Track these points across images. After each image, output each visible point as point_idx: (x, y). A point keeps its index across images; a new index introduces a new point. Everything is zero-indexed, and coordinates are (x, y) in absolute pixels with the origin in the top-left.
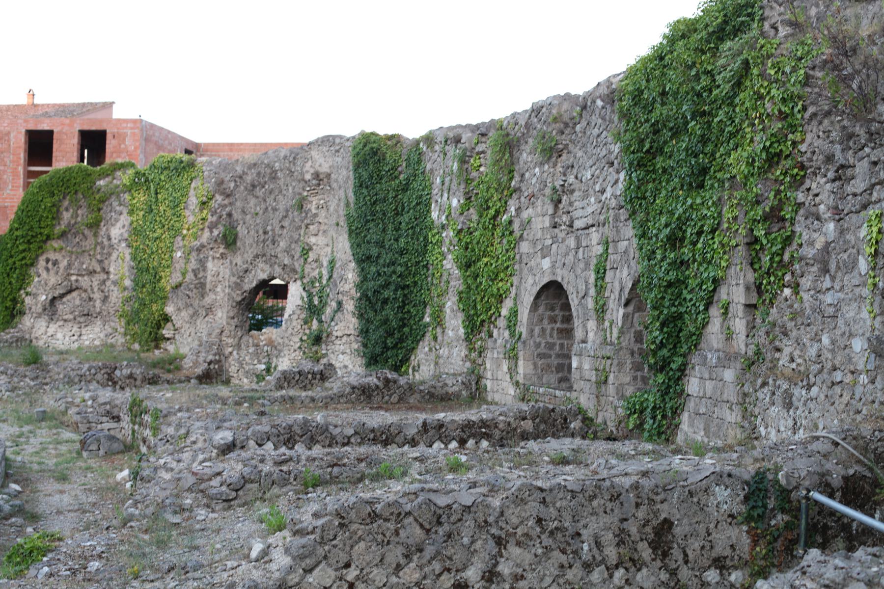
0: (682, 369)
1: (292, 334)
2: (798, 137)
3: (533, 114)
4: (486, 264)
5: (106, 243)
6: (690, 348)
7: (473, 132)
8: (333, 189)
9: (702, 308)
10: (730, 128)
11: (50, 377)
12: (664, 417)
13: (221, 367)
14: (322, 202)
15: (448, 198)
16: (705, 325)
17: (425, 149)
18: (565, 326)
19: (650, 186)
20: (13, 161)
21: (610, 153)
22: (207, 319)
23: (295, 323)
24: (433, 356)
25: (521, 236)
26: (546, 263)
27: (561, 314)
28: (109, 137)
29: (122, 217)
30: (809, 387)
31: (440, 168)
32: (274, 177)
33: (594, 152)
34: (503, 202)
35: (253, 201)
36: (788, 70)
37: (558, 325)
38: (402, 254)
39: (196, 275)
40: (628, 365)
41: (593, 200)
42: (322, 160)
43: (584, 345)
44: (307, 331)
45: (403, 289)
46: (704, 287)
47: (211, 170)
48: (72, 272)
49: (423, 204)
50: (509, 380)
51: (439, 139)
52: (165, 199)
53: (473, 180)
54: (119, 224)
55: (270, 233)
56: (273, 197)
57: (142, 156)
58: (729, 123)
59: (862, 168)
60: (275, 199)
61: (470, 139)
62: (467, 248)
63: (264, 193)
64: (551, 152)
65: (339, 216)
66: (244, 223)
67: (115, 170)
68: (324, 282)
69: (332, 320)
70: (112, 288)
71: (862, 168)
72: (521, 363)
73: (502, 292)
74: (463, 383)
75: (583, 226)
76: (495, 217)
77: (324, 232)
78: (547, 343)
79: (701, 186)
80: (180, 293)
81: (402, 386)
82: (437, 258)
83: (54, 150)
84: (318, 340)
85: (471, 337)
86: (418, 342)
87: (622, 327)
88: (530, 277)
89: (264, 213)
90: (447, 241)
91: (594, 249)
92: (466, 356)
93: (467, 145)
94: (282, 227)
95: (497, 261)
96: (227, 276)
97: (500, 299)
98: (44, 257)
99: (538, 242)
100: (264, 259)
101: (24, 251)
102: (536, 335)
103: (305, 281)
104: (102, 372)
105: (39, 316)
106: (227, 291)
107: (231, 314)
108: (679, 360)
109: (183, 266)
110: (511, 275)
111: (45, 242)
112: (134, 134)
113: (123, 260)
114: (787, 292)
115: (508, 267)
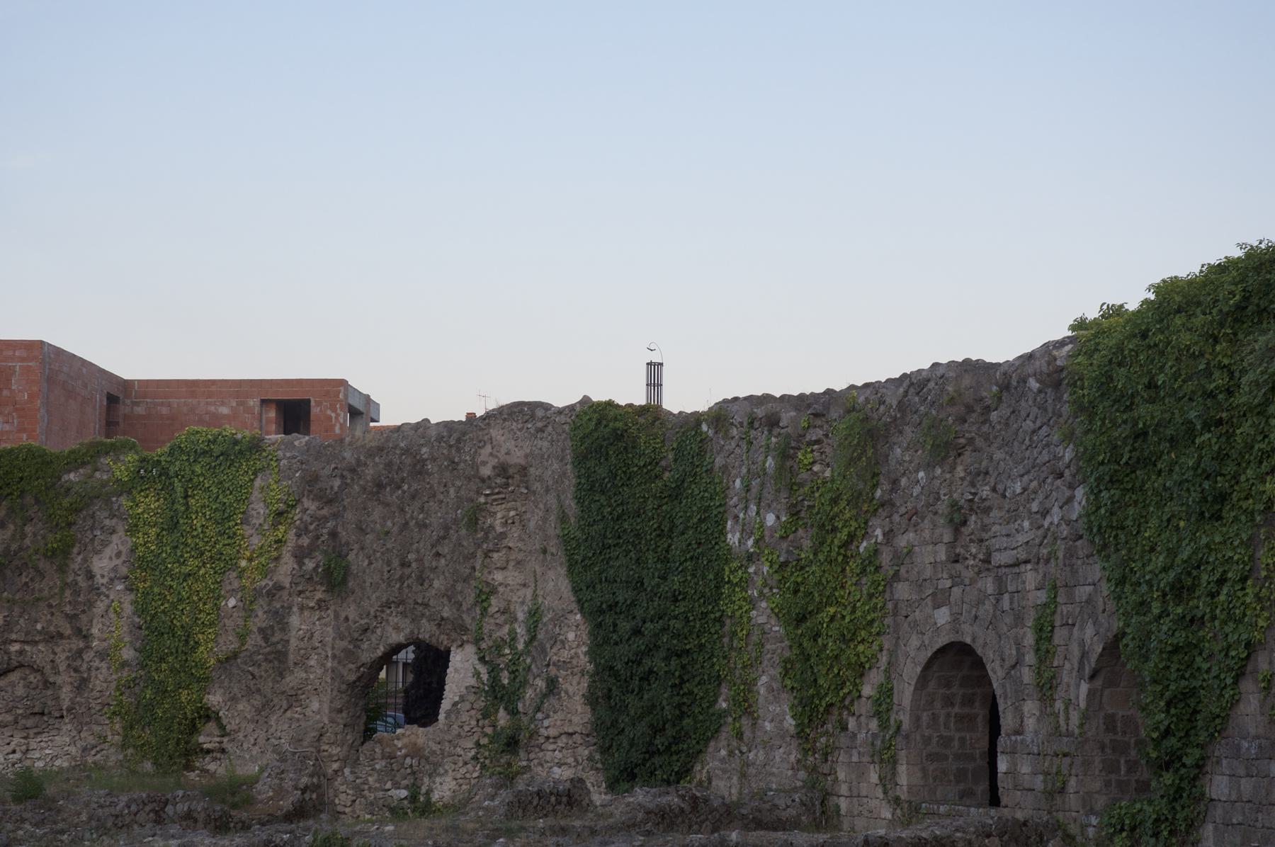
0: (1199, 766)
1: (459, 735)
3: (912, 390)
4: (832, 619)
5: (82, 582)
6: (1212, 735)
7: (797, 409)
8: (534, 493)
9: (1229, 681)
10: (1262, 446)
11: (64, 820)
12: (1172, 833)
13: (321, 796)
14: (512, 513)
15: (758, 513)
16: (1235, 702)
17: (711, 433)
18: (966, 710)
19: (1131, 511)
21: (1058, 458)
22: (289, 714)
23: (465, 717)
24: (736, 764)
25: (896, 573)
26: (942, 616)
27: (961, 692)
29: (115, 538)
31: (737, 469)
32: (419, 470)
33: (1027, 454)
34: (861, 520)
35: (377, 512)
37: (956, 709)
38: (676, 600)
39: (266, 639)
41: (1026, 524)
42: (510, 445)
43: (1019, 738)
44: (489, 730)
45: (679, 656)
46: (1233, 653)
47: (294, 457)
48: (14, 637)
49: (713, 521)
50: (881, 796)
51: (738, 419)
52: (203, 506)
53: (801, 485)
54: (108, 552)
55: (414, 565)
56: (417, 504)
57: (43, 411)
58: (1260, 438)
60: (422, 509)
62: (796, 592)
64: (944, 450)
66: (362, 548)
68: (521, 646)
69: (538, 709)
70: (97, 663)
72: (902, 768)
73: (863, 660)
74: (803, 804)
75: (1010, 562)
76: (845, 545)
77: (519, 563)
78: (941, 737)
80: (235, 671)
81: (716, 809)
82: (740, 608)
85: (808, 730)
86: (708, 740)
87: (1087, 709)
88: (914, 637)
89: (401, 531)
90: (759, 581)
91: (1030, 596)
92: (798, 761)
93: (789, 430)
94: (438, 555)
95: (853, 612)
96: (329, 639)
97: (861, 670)
99: (927, 584)
100: (401, 609)
102: (924, 724)
103: (484, 646)
104: (147, 808)
106: (329, 664)
108: (1197, 753)
109: (241, 622)
110: (878, 634)
113: (118, 614)
115: (873, 621)
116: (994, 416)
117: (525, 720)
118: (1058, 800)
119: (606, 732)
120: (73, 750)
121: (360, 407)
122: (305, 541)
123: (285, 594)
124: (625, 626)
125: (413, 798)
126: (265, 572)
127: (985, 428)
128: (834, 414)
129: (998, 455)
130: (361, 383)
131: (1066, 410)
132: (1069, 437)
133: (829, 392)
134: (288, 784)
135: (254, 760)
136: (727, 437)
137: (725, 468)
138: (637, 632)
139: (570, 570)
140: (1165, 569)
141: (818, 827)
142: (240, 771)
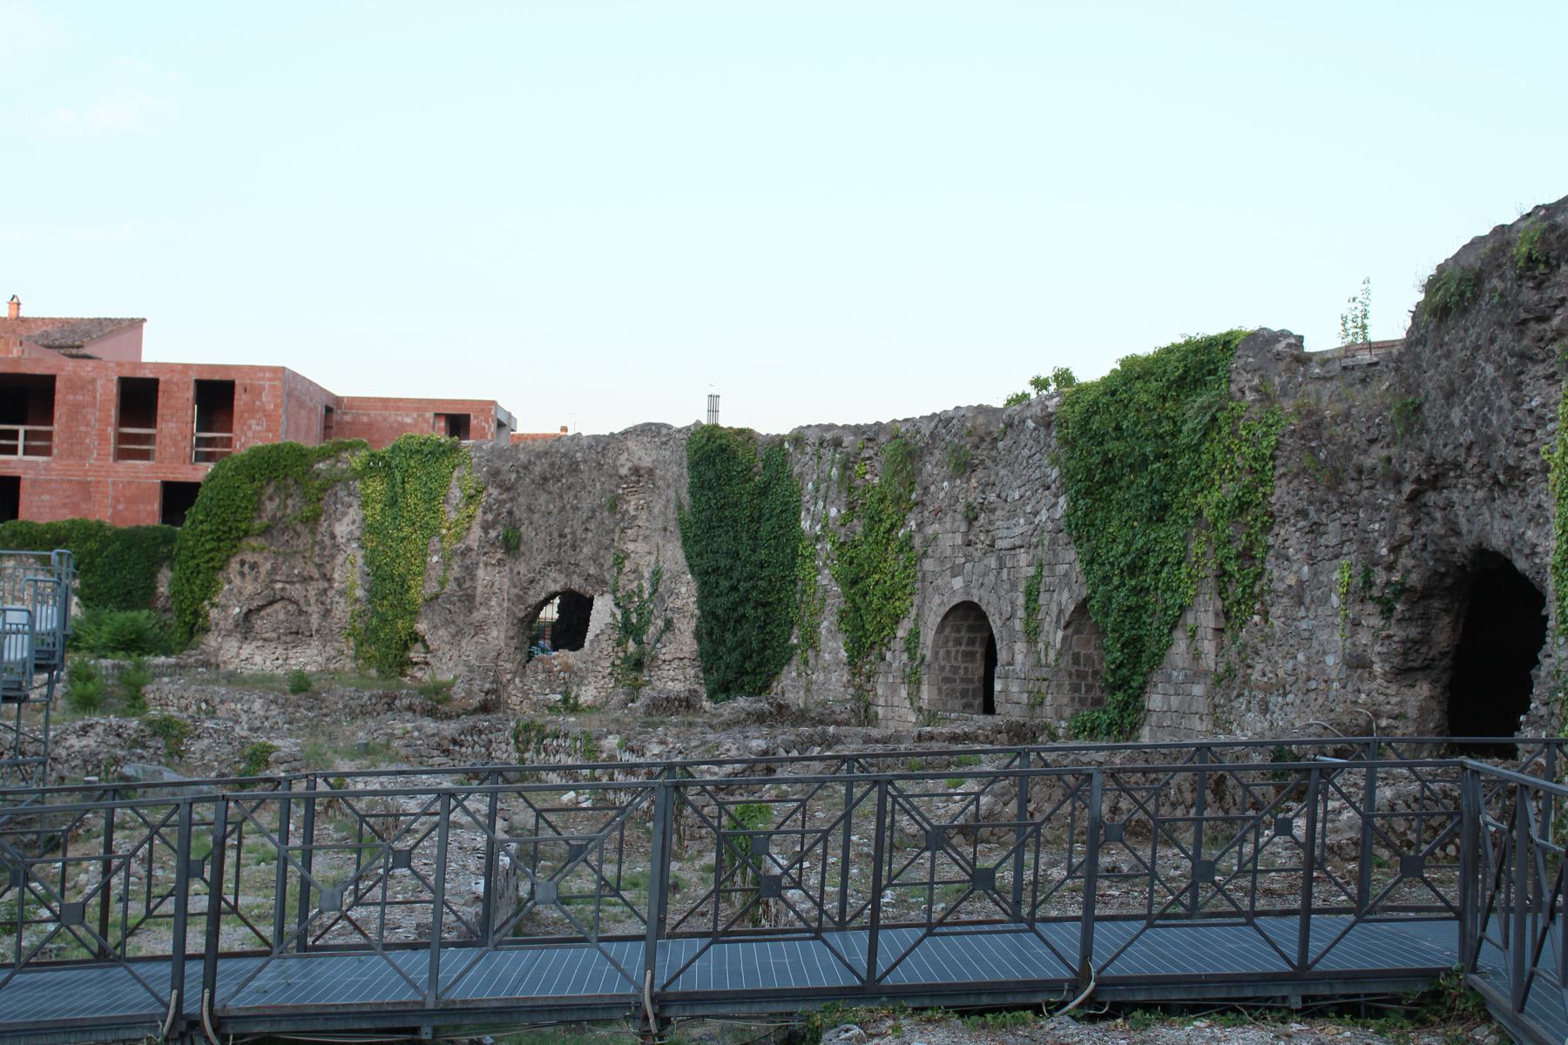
0: (1142, 688)
2: (1268, 490)
4: (877, 583)
5: (328, 542)
13: (498, 697)
16: (1169, 645)
19: (1099, 514)
20: (100, 420)
23: (604, 645)
24: (803, 682)
26: (958, 583)
28: (238, 390)
30: (1285, 695)
31: (809, 474)
32: (574, 468)
35: (543, 498)
36: (1259, 433)
37: (963, 648)
39: (459, 585)
40: (1067, 687)
41: (1022, 521)
42: (642, 453)
44: (621, 655)
49: (791, 512)
51: (811, 440)
53: (856, 488)
54: (347, 520)
56: (572, 493)
59: (1333, 527)
61: (852, 443)
62: (851, 563)
63: (560, 489)
65: (667, 520)
67: (340, 450)
68: (646, 596)
69: (658, 641)
70: (337, 599)
71: (1333, 527)
72: (925, 688)
76: (889, 531)
79: (1161, 520)
83: (160, 405)
84: (638, 665)
97: (896, 619)
98: (238, 558)
101: (211, 550)
105: (229, 634)
107: (511, 634)
108: (1141, 679)
111: (239, 539)
112: (274, 387)
114: (1256, 618)
116: (1000, 445)
117: (648, 648)
118: (1038, 710)
119: (708, 658)
120: (319, 659)
121: (504, 420)
122: (490, 517)
123: (473, 554)
124: (725, 584)
125: (565, 701)
126: (460, 538)
127: (994, 453)
128: (882, 439)
129: (1002, 472)
130: (506, 404)
131: (1054, 443)
132: (1055, 462)
133: (878, 424)
134: (476, 688)
135: (449, 670)
136: (804, 453)
137: (801, 475)
138: (734, 588)
139: (684, 544)
140: (1123, 555)
141: (860, 724)
142: (439, 678)
